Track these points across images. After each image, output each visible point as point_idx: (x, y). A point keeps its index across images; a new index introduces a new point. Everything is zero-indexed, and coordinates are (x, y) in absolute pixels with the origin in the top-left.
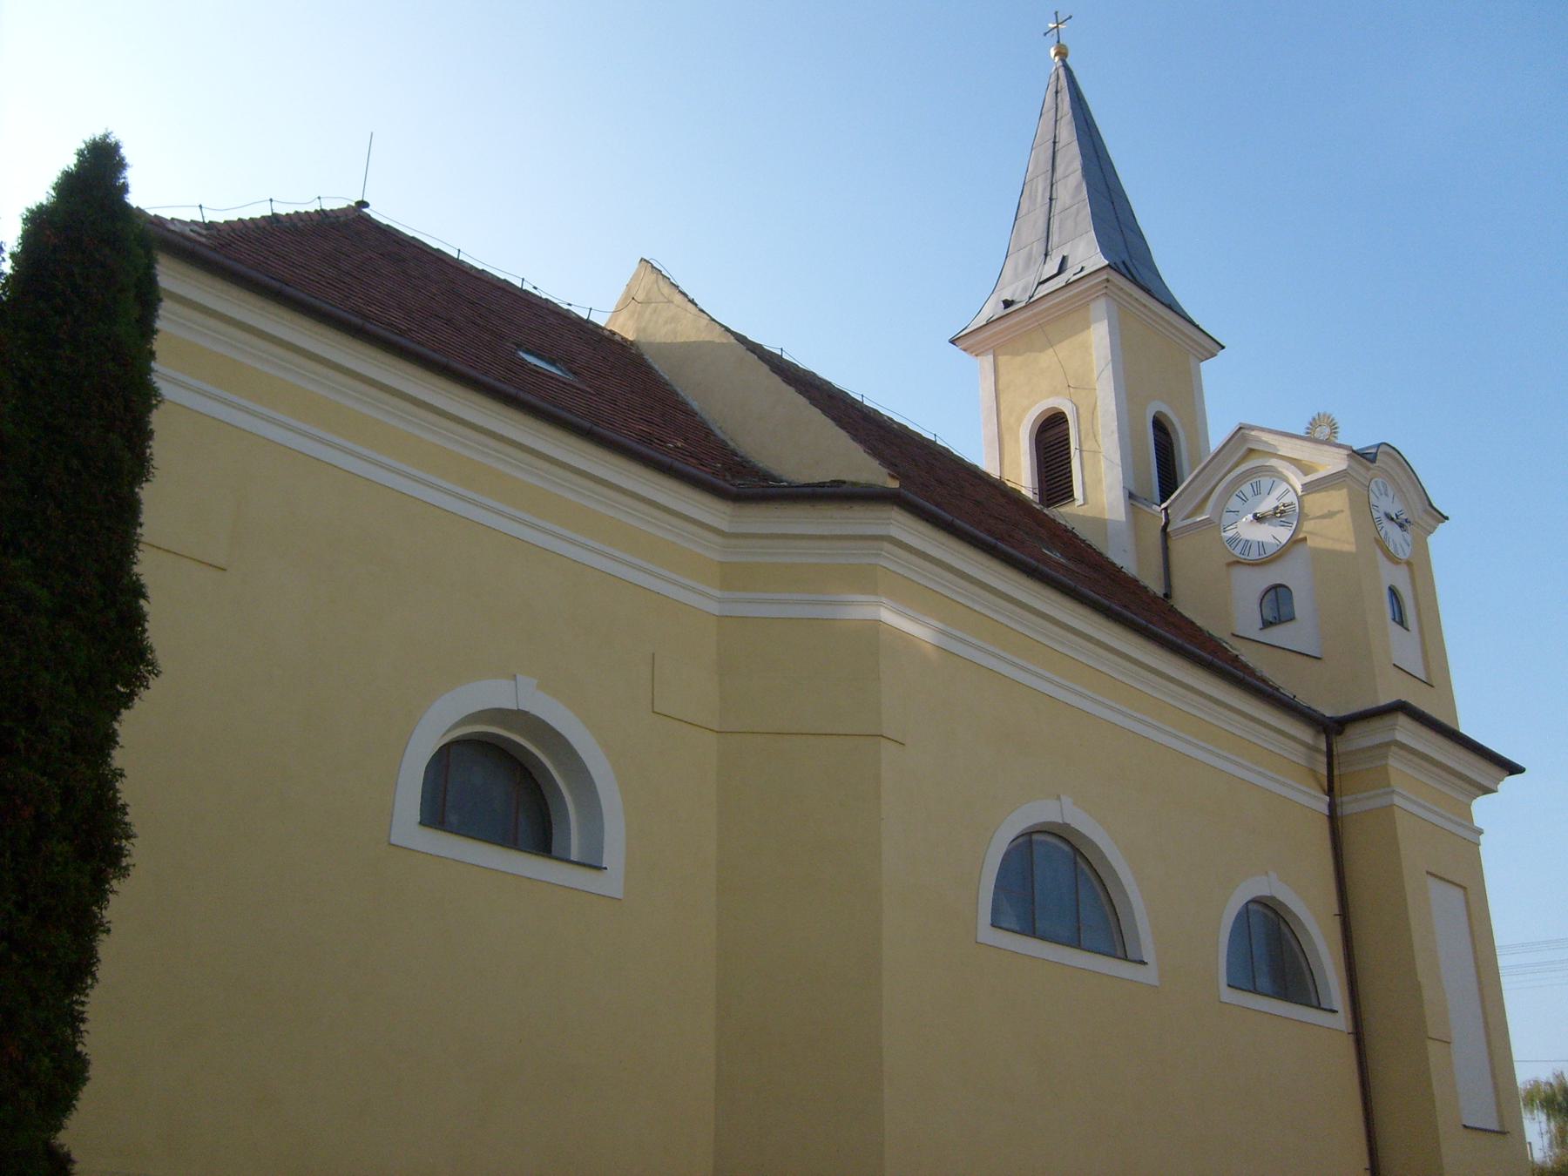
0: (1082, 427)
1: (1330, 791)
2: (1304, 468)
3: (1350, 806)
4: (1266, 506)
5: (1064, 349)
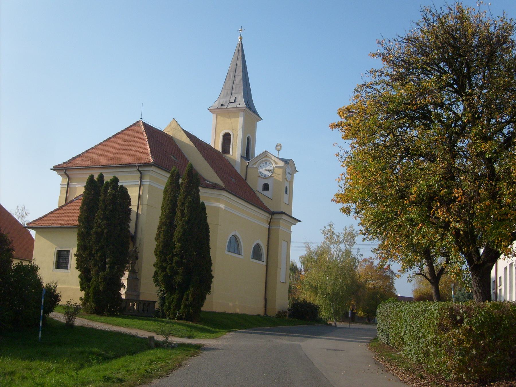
0: (234, 139)
1: (269, 224)
2: (276, 163)
3: (273, 227)
4: (268, 168)
5: (233, 120)
